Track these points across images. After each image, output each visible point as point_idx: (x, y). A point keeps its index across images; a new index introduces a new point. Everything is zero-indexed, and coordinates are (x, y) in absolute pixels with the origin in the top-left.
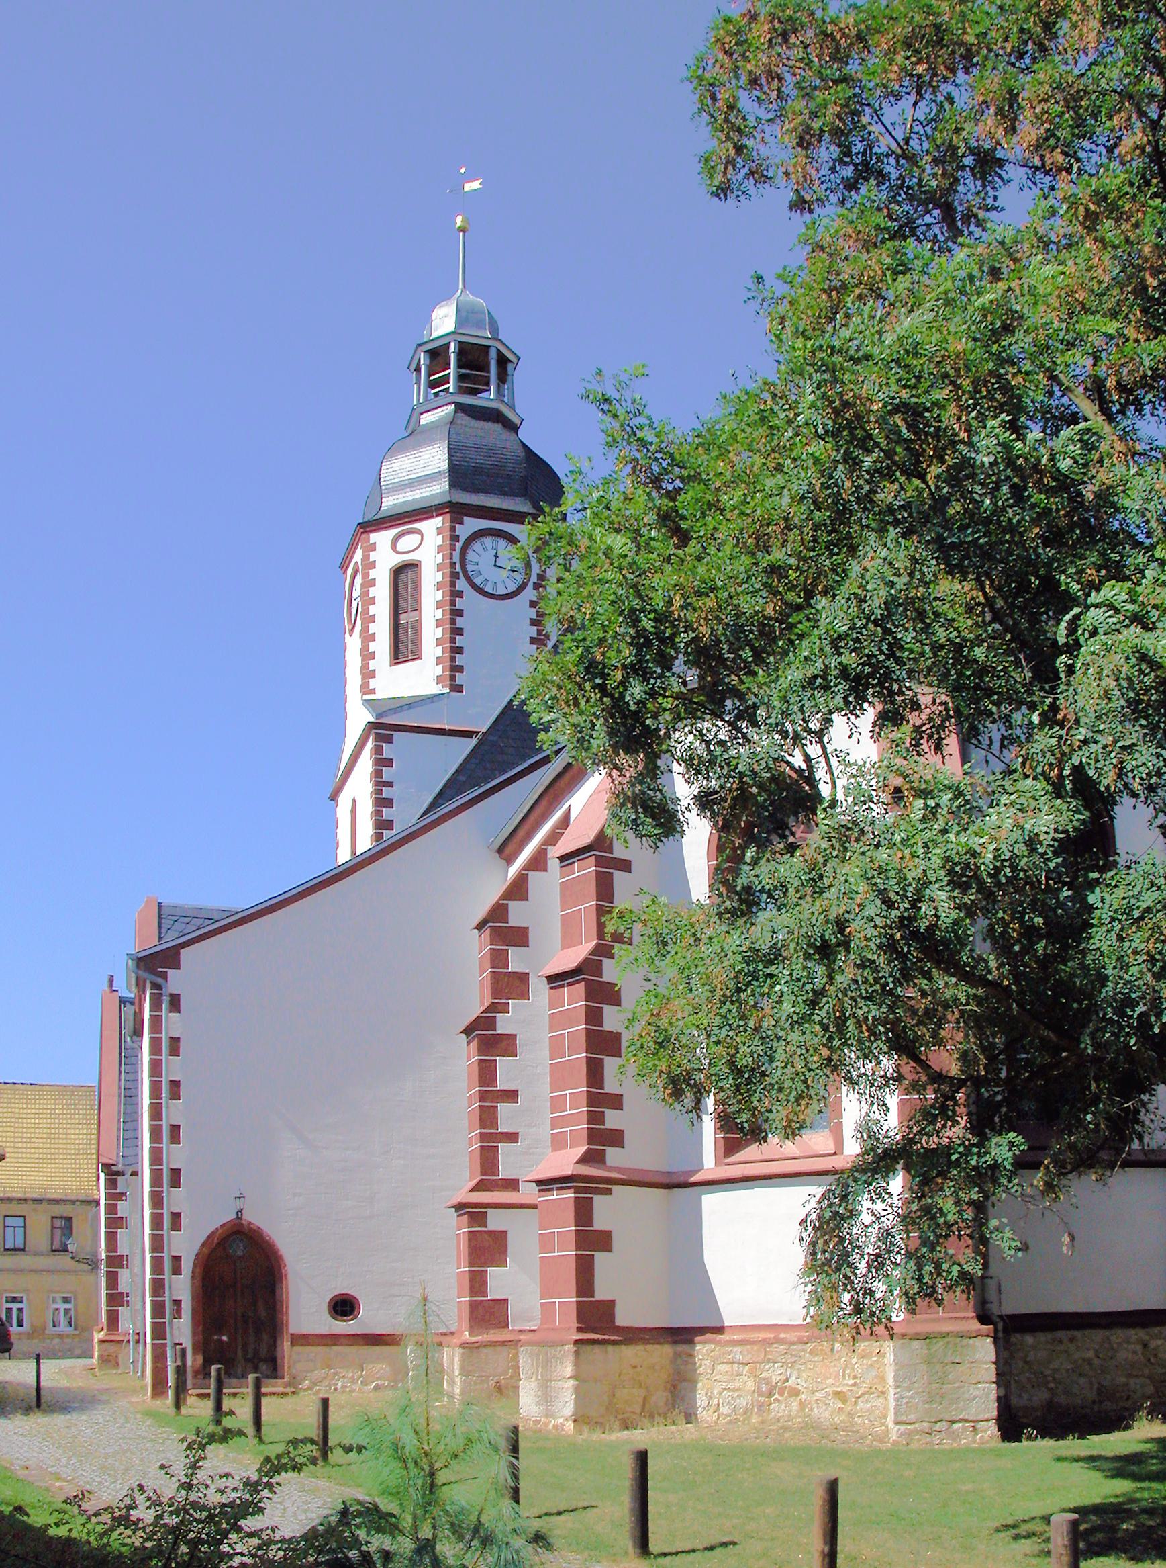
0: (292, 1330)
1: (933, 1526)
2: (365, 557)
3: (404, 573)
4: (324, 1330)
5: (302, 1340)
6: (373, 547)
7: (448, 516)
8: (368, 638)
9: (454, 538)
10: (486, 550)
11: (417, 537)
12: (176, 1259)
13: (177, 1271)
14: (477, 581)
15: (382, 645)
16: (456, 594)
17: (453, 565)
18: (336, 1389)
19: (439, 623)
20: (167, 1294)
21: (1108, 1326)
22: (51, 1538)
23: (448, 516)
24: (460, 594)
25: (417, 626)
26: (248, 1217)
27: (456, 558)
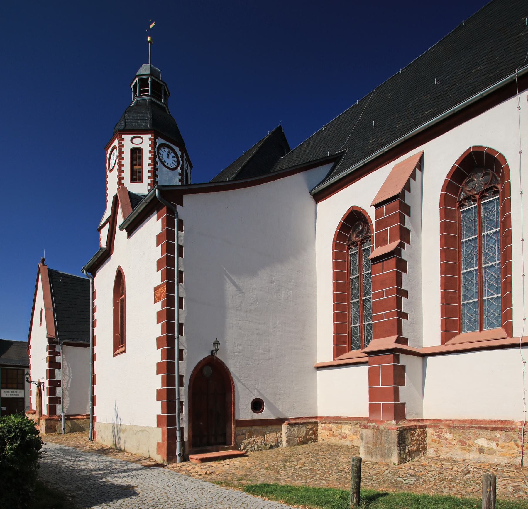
0: (236, 418)
1: (395, 487)
2: (120, 143)
3: (136, 153)
4: (249, 418)
5: (241, 423)
6: (123, 140)
7: (153, 134)
8: (120, 172)
9: (155, 143)
10: (165, 151)
11: (141, 140)
12: (181, 377)
13: (181, 385)
14: (163, 161)
15: (127, 175)
16: (155, 163)
17: (155, 152)
18: (255, 449)
19: (149, 171)
20: (177, 398)
21: (251, 426)
22: (149, 133)
23: (153, 134)
24: (157, 163)
25: (140, 171)
26: (218, 355)
27: (156, 150)
